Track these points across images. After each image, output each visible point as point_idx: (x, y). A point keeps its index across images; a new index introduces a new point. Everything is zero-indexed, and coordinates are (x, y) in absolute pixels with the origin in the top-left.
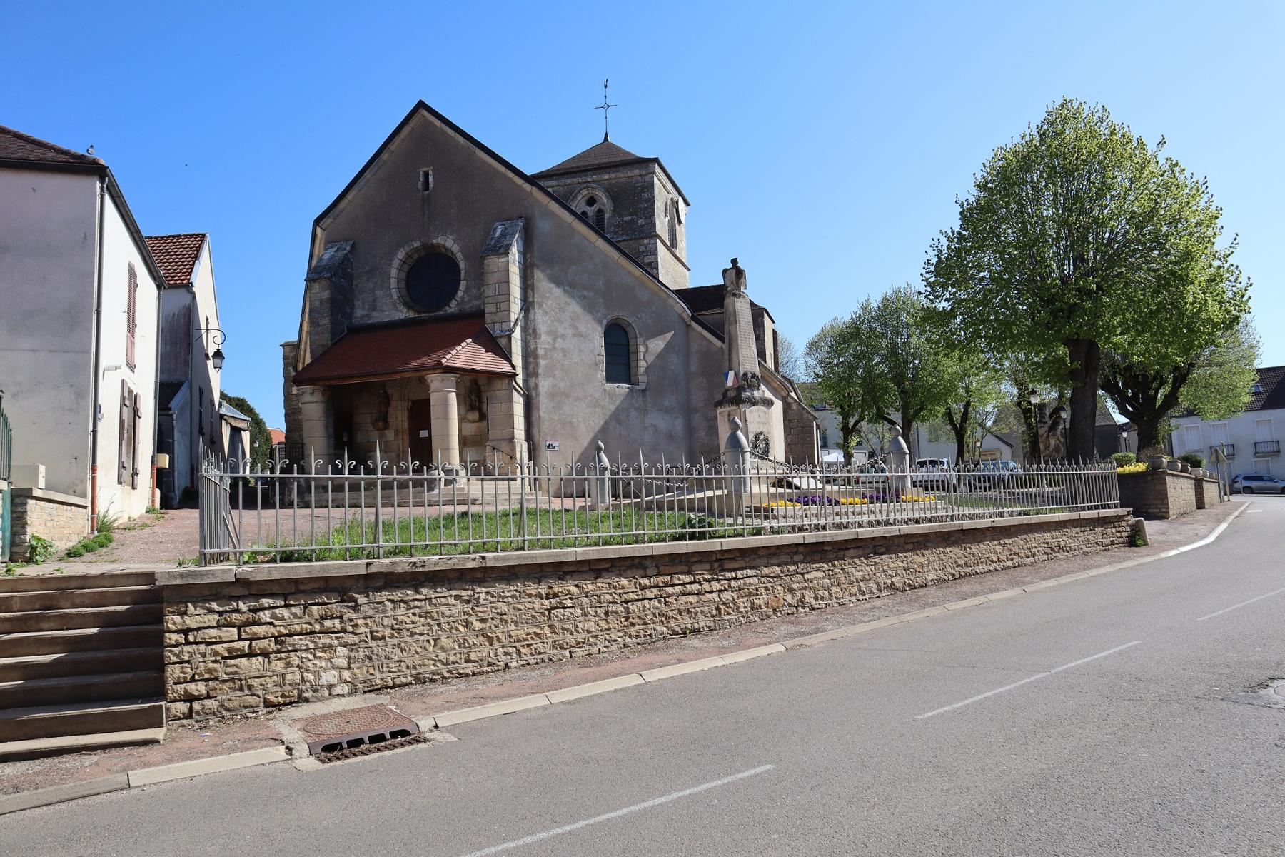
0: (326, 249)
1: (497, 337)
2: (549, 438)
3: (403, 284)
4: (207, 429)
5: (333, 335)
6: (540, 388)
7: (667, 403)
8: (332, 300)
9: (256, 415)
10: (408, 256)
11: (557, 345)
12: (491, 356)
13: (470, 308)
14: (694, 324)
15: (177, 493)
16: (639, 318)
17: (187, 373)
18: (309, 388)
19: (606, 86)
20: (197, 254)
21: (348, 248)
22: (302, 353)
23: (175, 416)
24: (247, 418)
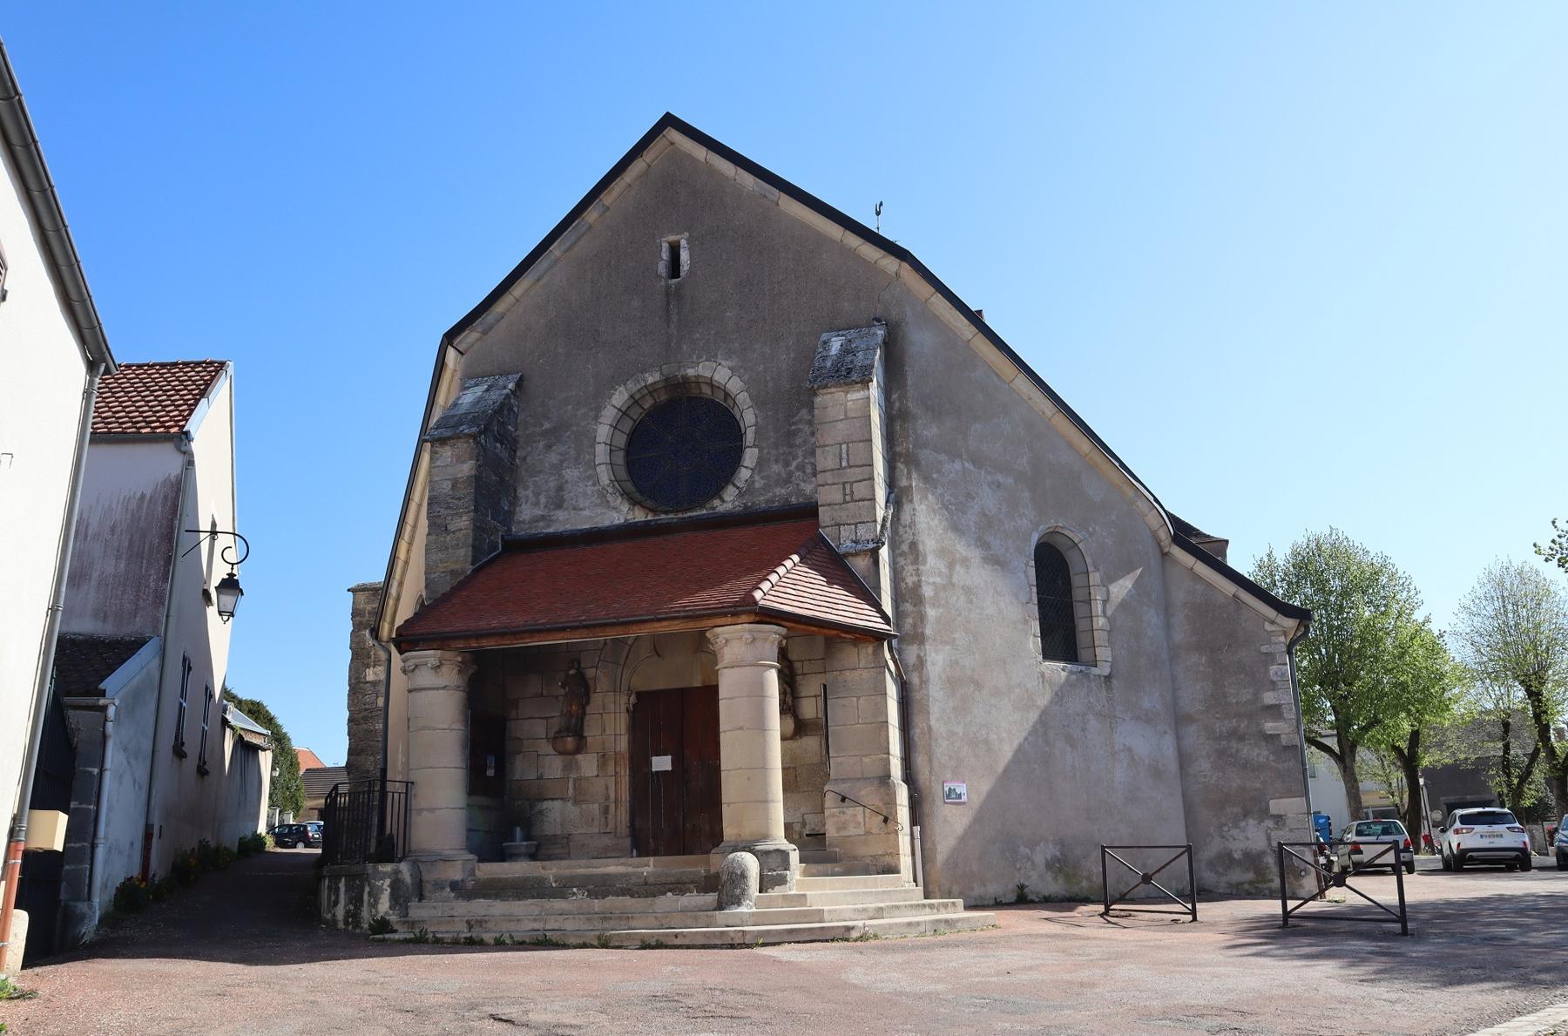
0: (464, 388)
1: (847, 555)
2: (949, 776)
3: (620, 458)
4: (191, 748)
5: (477, 550)
6: (929, 666)
7: (1146, 705)
8: (477, 480)
9: (277, 726)
10: (635, 401)
12: (838, 592)
13: (767, 501)
14: (1177, 552)
15: (96, 900)
16: (1091, 534)
17: (156, 621)
18: (430, 656)
19: (878, 213)
20: (205, 390)
21: (511, 386)
22: (391, 602)
23: (111, 711)
24: (265, 732)
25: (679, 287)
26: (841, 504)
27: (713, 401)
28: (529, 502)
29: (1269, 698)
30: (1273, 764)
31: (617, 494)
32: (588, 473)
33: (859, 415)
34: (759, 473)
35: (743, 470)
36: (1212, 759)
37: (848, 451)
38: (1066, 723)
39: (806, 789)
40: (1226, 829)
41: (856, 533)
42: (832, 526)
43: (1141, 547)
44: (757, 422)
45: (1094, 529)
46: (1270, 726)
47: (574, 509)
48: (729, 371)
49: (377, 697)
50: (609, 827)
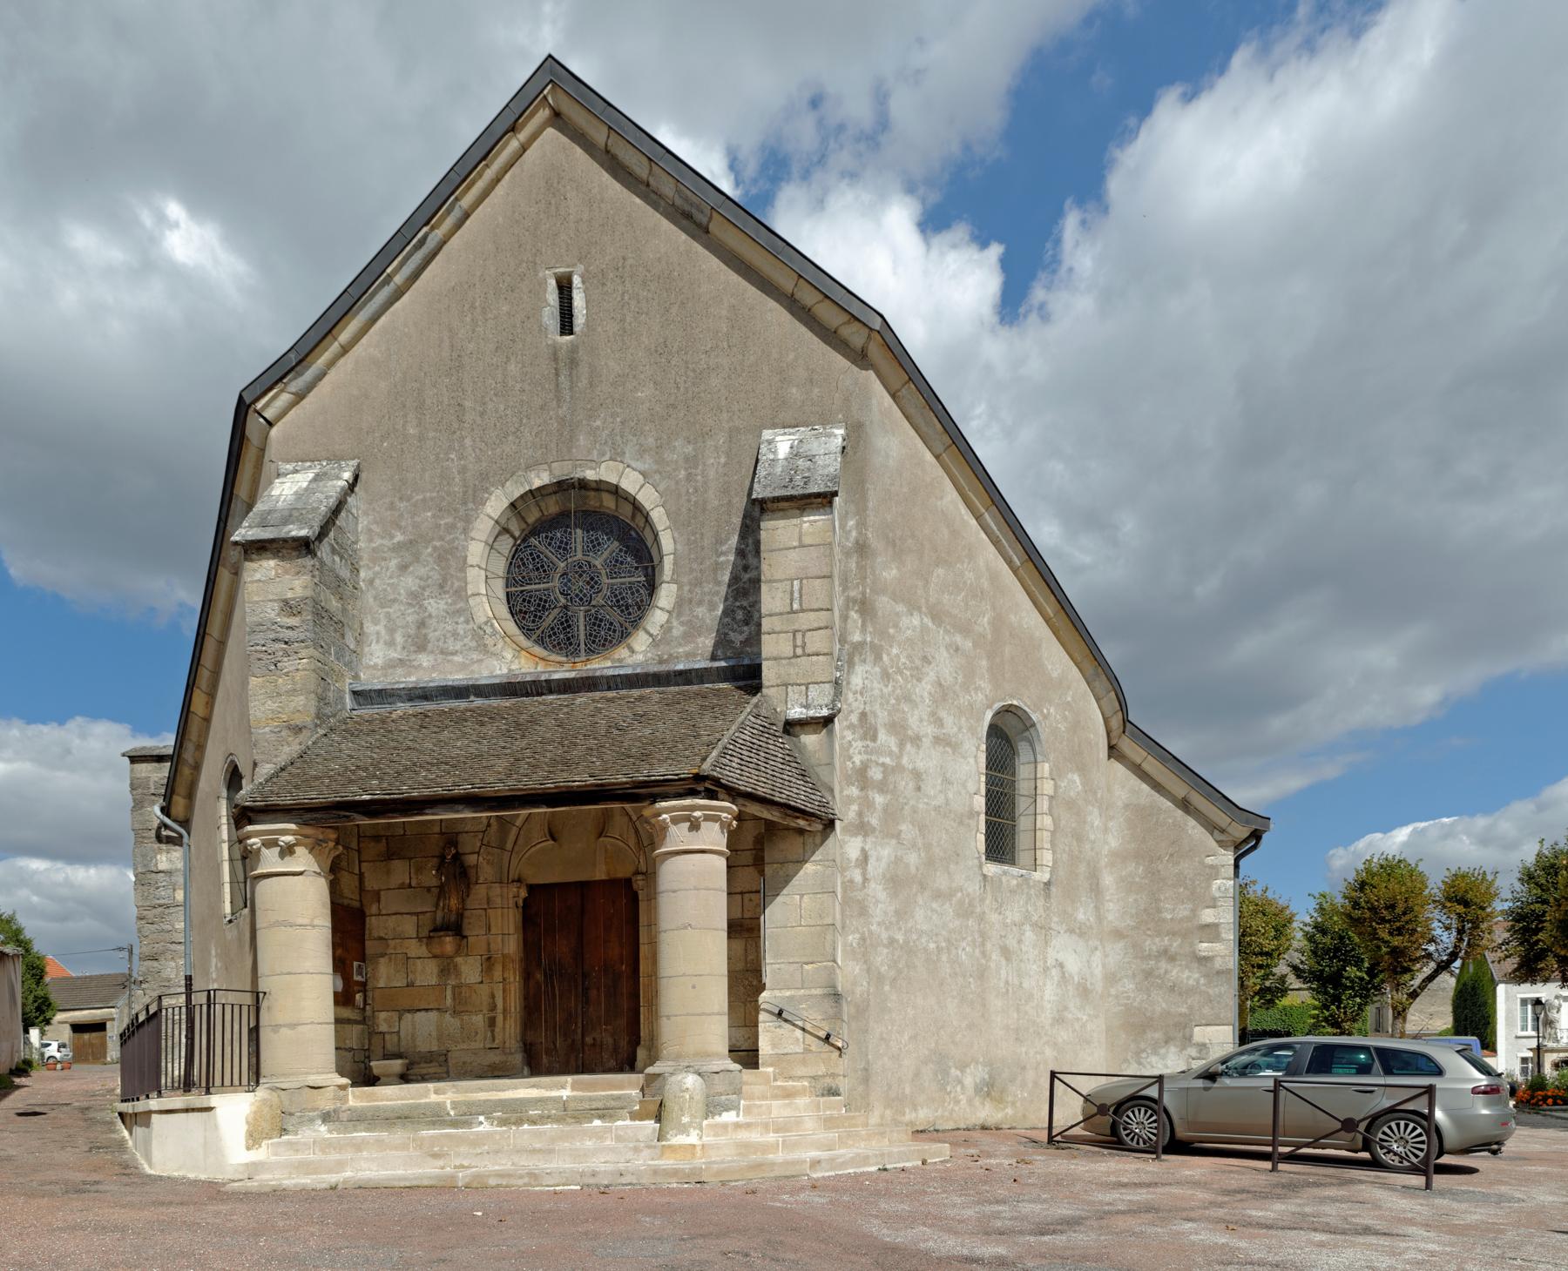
7: (1081, 916)
11: (905, 761)
25: (574, 349)
26: (790, 658)
27: (616, 518)
28: (382, 641)
29: (1208, 916)
30: (1203, 988)
31: (498, 636)
32: (458, 606)
33: (818, 541)
34: (679, 615)
35: (658, 612)
37: (801, 589)
38: (1003, 934)
40: (1144, 1055)
41: (807, 697)
42: (778, 686)
43: (1092, 736)
44: (675, 549)
45: (1048, 710)
46: (1204, 948)
47: (442, 652)
48: (641, 477)
49: (174, 890)
50: (497, 1041)
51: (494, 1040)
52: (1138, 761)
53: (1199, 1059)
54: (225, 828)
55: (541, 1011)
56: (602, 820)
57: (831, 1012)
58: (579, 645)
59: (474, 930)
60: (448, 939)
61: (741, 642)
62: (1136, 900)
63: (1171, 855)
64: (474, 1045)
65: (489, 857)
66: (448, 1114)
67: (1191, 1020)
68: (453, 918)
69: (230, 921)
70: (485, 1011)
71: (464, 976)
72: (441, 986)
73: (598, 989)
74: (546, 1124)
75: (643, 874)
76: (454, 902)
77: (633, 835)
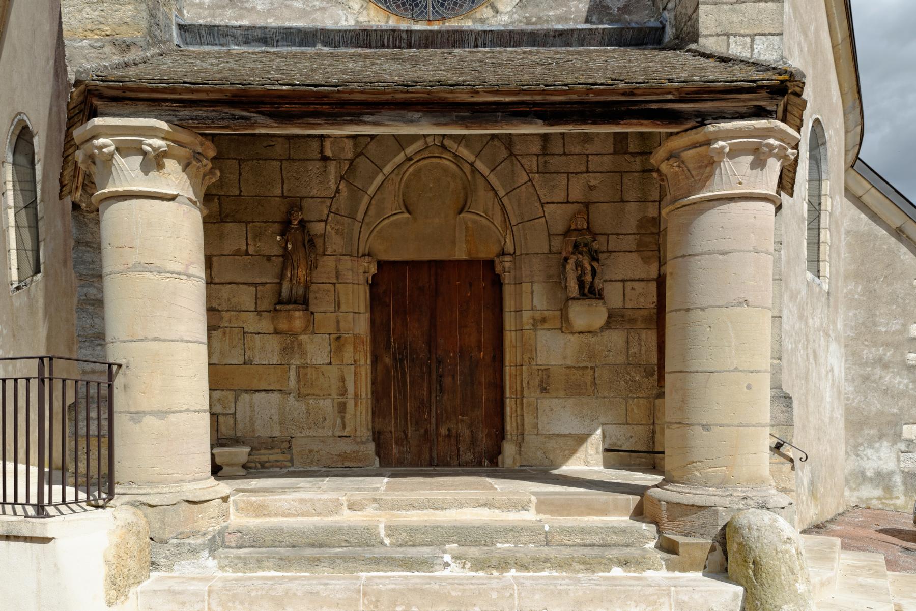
36: (856, 383)
39: (606, 394)
40: (861, 448)
42: (718, 35)
51: (344, 428)
52: (860, 192)
53: (907, 452)
54: (10, 194)
55: (390, 397)
56: (462, 195)
57: (782, 417)
58: (426, 7)
59: (322, 306)
60: (297, 314)
61: (619, 9)
62: (855, 314)
63: (886, 277)
64: (321, 432)
65: (338, 227)
66: (382, 543)
67: (901, 420)
68: (301, 291)
69: (18, 288)
70: (334, 396)
71: (309, 355)
72: (284, 367)
73: (453, 377)
74: (543, 570)
75: (510, 254)
76: (302, 273)
77: (498, 209)
